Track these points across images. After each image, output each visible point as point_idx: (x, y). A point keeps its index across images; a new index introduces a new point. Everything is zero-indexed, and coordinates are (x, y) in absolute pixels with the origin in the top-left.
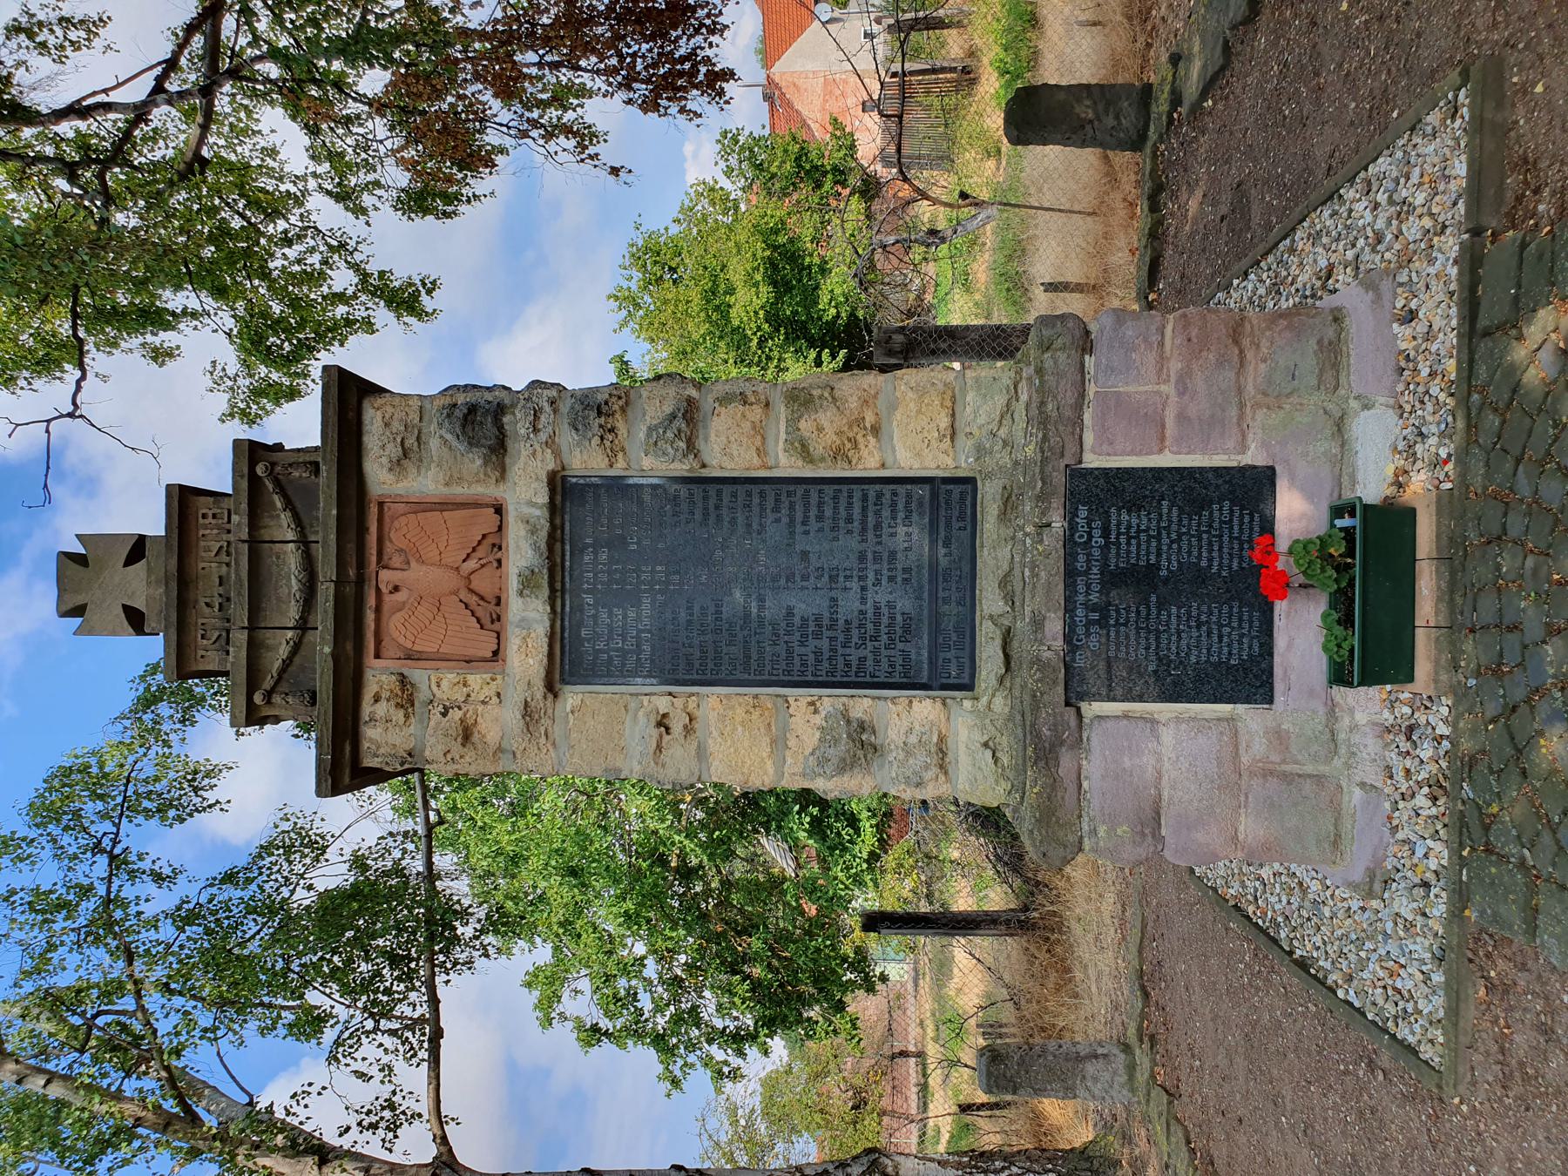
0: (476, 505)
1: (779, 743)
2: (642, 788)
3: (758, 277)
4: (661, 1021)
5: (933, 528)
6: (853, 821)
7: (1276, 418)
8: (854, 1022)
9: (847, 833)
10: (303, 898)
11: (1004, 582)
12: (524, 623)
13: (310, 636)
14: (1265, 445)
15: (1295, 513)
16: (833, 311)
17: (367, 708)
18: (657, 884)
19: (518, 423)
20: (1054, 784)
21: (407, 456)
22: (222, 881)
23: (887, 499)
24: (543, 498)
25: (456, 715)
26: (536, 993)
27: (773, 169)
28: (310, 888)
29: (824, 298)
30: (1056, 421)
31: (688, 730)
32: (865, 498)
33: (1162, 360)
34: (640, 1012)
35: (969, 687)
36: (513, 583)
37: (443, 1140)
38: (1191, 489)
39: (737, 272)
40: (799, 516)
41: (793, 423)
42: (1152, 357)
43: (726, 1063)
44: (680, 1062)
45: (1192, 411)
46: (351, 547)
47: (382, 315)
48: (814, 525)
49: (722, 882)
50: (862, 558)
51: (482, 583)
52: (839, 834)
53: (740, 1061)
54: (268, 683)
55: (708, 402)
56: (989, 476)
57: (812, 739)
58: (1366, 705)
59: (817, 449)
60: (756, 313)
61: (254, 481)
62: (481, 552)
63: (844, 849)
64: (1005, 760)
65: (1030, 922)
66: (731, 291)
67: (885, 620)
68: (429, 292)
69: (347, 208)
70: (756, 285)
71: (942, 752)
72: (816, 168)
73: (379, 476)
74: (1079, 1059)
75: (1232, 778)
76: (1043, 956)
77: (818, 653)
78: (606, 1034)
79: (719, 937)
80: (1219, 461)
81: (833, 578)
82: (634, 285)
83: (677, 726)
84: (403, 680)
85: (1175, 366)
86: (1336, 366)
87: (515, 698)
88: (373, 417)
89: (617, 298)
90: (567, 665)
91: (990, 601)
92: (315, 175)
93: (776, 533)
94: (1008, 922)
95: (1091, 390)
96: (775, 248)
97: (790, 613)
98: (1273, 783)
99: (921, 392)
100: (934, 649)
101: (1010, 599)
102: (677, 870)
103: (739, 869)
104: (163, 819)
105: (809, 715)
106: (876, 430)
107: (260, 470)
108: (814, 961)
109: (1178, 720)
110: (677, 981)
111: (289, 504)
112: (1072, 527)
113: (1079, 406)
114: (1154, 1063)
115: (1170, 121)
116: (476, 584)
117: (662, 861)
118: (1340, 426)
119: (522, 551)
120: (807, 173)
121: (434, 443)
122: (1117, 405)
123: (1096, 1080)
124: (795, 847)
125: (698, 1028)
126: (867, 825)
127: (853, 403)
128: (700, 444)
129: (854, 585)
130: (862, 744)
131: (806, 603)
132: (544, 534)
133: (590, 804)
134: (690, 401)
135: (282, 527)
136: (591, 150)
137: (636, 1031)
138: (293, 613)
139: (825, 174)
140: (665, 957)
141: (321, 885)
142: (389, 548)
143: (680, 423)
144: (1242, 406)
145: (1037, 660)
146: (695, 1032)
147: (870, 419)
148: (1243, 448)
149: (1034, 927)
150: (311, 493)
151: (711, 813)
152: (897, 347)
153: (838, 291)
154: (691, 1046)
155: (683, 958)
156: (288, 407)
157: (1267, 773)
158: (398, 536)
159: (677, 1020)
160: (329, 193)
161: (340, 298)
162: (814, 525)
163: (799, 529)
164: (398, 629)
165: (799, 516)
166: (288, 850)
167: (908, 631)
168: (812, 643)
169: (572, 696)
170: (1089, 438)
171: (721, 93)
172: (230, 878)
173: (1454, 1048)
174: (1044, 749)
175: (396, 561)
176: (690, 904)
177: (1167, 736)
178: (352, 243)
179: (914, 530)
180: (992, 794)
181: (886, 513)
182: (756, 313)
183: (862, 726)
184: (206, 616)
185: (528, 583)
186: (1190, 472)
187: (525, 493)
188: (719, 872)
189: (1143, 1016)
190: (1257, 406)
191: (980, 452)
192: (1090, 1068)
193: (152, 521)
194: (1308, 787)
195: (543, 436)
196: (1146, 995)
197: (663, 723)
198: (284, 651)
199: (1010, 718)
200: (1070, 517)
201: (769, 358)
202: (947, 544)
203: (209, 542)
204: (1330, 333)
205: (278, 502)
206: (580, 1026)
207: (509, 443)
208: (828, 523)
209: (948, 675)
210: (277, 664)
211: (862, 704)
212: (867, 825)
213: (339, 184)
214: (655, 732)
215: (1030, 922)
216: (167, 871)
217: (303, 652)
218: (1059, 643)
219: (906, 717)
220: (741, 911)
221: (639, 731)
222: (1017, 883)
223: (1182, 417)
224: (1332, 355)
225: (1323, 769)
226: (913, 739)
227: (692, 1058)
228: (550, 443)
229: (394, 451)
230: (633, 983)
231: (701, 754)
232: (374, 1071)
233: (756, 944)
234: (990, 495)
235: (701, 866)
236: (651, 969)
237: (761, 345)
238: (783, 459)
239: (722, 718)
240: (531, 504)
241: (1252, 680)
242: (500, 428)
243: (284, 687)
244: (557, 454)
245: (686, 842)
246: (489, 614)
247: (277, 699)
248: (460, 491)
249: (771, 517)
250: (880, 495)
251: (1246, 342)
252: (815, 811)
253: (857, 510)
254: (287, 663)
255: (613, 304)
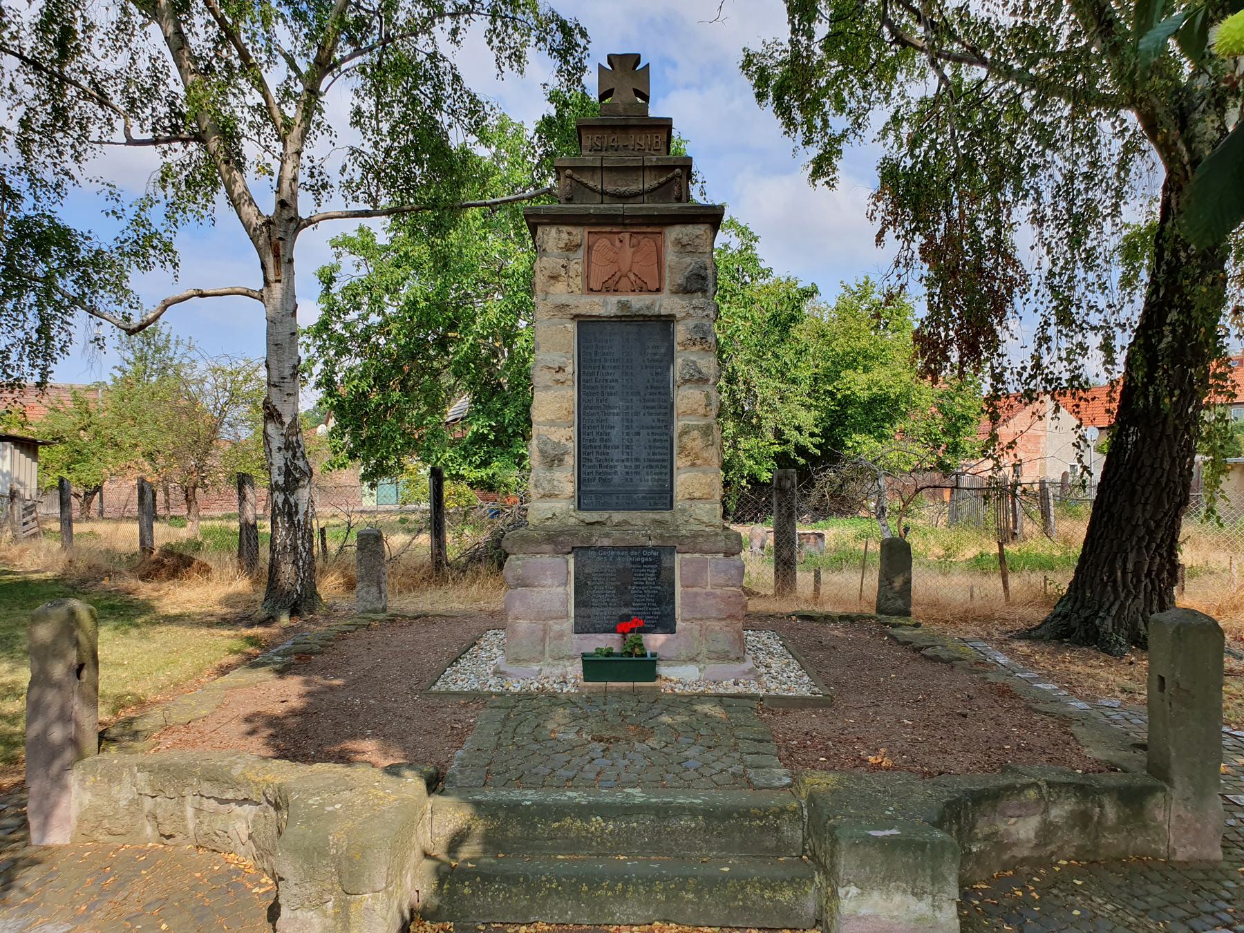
0: (661, 279)
1: (552, 423)
2: (505, 312)
3: (875, 390)
4: (338, 327)
5: (651, 492)
6: (485, 463)
7: (696, 634)
8: (343, 465)
9: (476, 459)
10: (444, 119)
11: (626, 522)
12: (605, 304)
13: (599, 198)
14: (684, 629)
15: (655, 641)
16: (850, 444)
17: (564, 229)
18: (435, 324)
19: (698, 300)
20: (538, 542)
21: (682, 246)
22: (454, 75)
23: (663, 470)
24: (663, 312)
25: (563, 272)
26: (355, 235)
27: (957, 399)
28: (450, 126)
29: (858, 437)
30: (694, 543)
31: (557, 381)
32: (664, 460)
33: (722, 586)
34: (346, 313)
35: (579, 508)
36: (624, 298)
37: (310, 222)
38: (666, 598)
39: (880, 374)
40: (656, 431)
41: (697, 427)
42: (722, 581)
43: (311, 375)
44: (309, 341)
45: (699, 599)
46: (640, 221)
47: (814, 151)
48: (652, 438)
49: (437, 370)
50: (637, 460)
51: (624, 283)
52: (476, 454)
53: (313, 384)
54: (576, 176)
55: (707, 389)
56: (673, 515)
57: (555, 438)
58: (575, 670)
59: (685, 439)
60: (849, 389)
61: (673, 168)
62: (638, 281)
63: (465, 458)
64: (548, 523)
65: (439, 568)
66: (866, 370)
67: (609, 471)
68: (827, 183)
69: (887, 124)
70: (869, 388)
71: (550, 496)
72: (958, 430)
73: (674, 233)
74: (379, 584)
75: (543, 617)
76: (419, 576)
77: (594, 440)
78: (328, 288)
79: (400, 369)
80: (678, 611)
81: (627, 447)
82: (874, 296)
83: (558, 376)
84: (579, 246)
85: (718, 591)
86: (718, 659)
87: (571, 300)
88: (701, 230)
89: (866, 283)
90: (585, 323)
91: (617, 516)
92: (908, 103)
93: (648, 420)
94: (440, 554)
95: (709, 557)
96: (897, 401)
97: (611, 427)
98: (541, 633)
99: (710, 485)
100: (596, 493)
101: (619, 524)
102: (445, 337)
103: (447, 380)
104: (490, 31)
105: (565, 436)
106: (693, 465)
107: (678, 170)
108: (385, 438)
109: (567, 594)
110: (367, 339)
111: (661, 185)
112: (649, 549)
113: (701, 551)
114: (381, 621)
115: (886, 624)
116: (624, 280)
117: (453, 326)
118: (693, 660)
119: (638, 302)
120: (955, 425)
121: (688, 260)
122: (703, 566)
123: (367, 593)
124: (465, 420)
125: (336, 354)
126: (483, 473)
127: (705, 455)
128: (688, 385)
129: (625, 457)
130: (553, 460)
131: (616, 435)
132: (647, 313)
133: (494, 274)
134: (708, 380)
135: (651, 182)
136: (924, 282)
137: (332, 310)
138: (610, 188)
139: (954, 438)
140: (383, 329)
141: (451, 133)
142: (640, 237)
143: (697, 376)
144: (701, 619)
145: (592, 535)
146: (332, 353)
147: (698, 462)
148: (683, 620)
149: (438, 570)
150: (665, 197)
151: (487, 362)
152: (783, 483)
153: (865, 448)
154: (322, 349)
155: (382, 341)
156: (752, 92)
157: (545, 631)
158: (647, 244)
159: (341, 340)
160: (897, 111)
161: (826, 123)
162: (652, 438)
163: (650, 431)
164: (603, 242)
165: (656, 431)
166: (473, 112)
167: (604, 481)
168: (598, 438)
169: (572, 327)
170: (687, 556)
171: (924, 378)
172: (457, 78)
173: (439, 694)
174: (554, 539)
175: (634, 241)
176: (422, 345)
177: (560, 590)
178: (860, 132)
179: (650, 483)
180: (533, 518)
181: (657, 470)
182: (849, 389)
183: (561, 460)
184: (609, 139)
185: (624, 305)
186: (673, 598)
187: (667, 303)
188: (445, 367)
189: (404, 617)
190: (701, 626)
191: (683, 511)
192: (374, 590)
193: (656, 110)
194: (540, 648)
195: (691, 312)
196: (416, 618)
197: (560, 369)
198: (591, 184)
199: (566, 525)
200: (654, 548)
201: (817, 399)
202: (644, 498)
203: (644, 140)
204: (732, 656)
205: (663, 180)
206: (334, 268)
207: (689, 295)
208: (652, 444)
209: (584, 499)
210: (585, 181)
211: (571, 461)
212: (483, 473)
213: (903, 118)
214: (556, 366)
215: (439, 568)
216: (458, 38)
217: (590, 193)
218: (599, 544)
219: (565, 480)
220: (416, 383)
221: (556, 358)
222: (463, 560)
223: (696, 595)
224: (723, 657)
225: (547, 655)
226: (556, 483)
227: (313, 350)
228: (688, 315)
229: (685, 240)
230: (365, 307)
231: (547, 388)
232: (347, 177)
233: (396, 395)
234: (666, 515)
235: (447, 354)
236: (375, 319)
237: (826, 392)
238: (681, 423)
239: (563, 397)
240: (660, 306)
241: (582, 628)
242: (695, 291)
243: (574, 184)
244: (683, 318)
245: (468, 345)
246: (609, 287)
247: (568, 181)
248: (667, 272)
249: (655, 418)
250: (665, 467)
251: (729, 621)
252: (492, 437)
253: (658, 457)
254: (586, 186)
255: (862, 281)
